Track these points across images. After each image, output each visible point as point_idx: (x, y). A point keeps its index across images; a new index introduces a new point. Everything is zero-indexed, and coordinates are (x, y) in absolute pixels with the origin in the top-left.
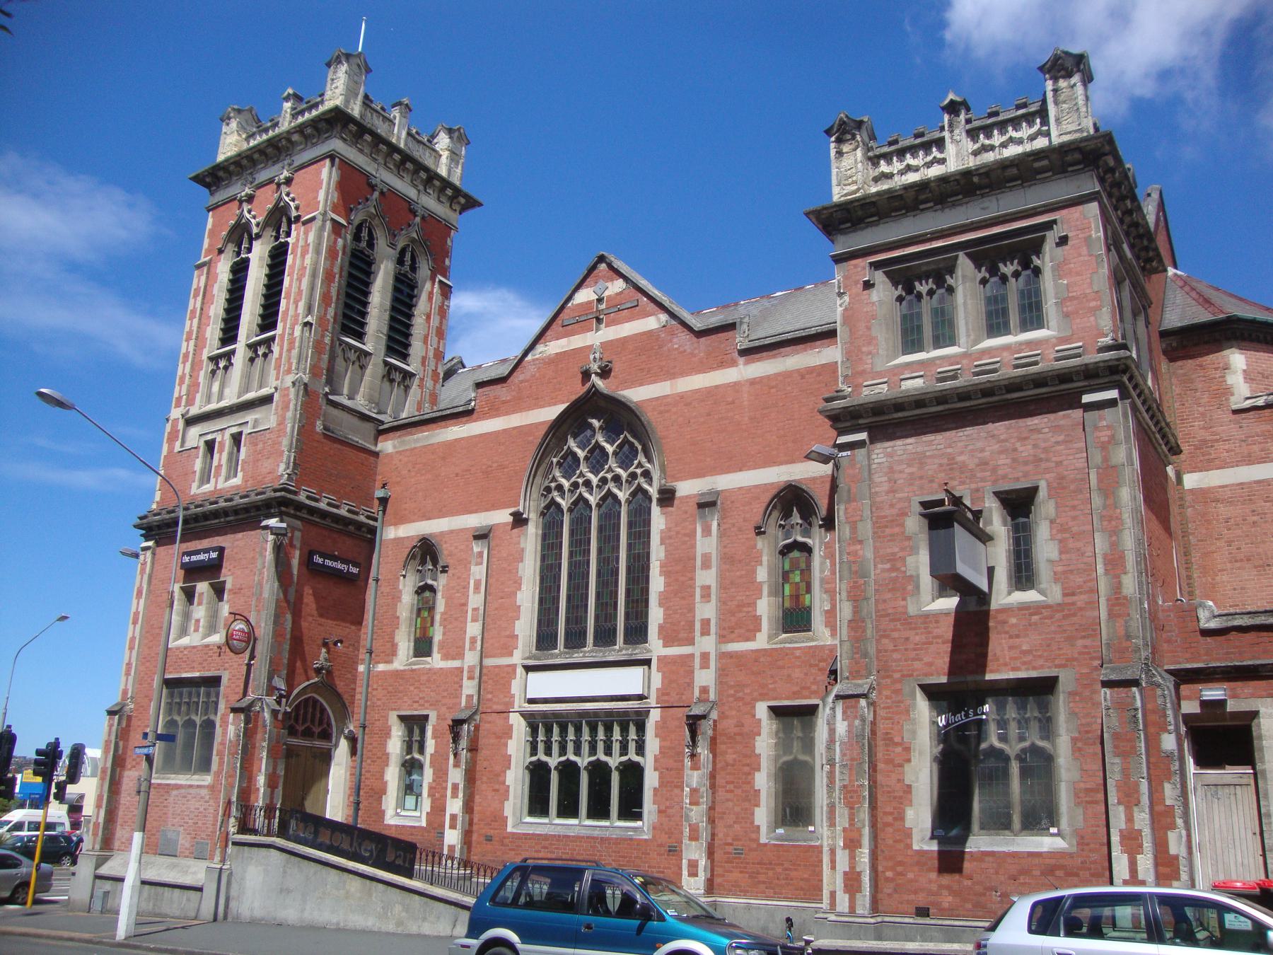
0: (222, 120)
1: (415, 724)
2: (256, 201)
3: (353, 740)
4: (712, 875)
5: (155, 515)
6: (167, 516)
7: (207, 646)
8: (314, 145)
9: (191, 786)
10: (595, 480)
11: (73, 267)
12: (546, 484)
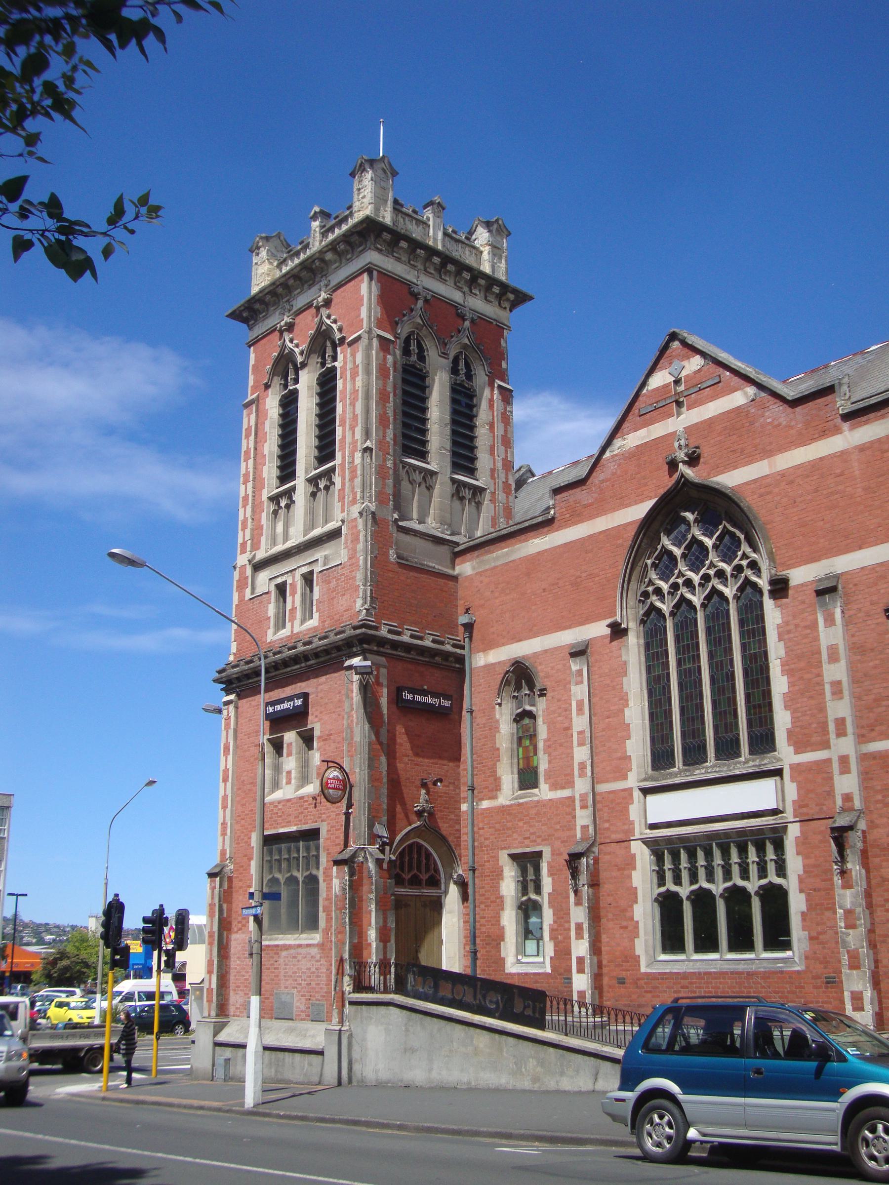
0: (251, 251)
1: (528, 862)
2: (296, 329)
3: (463, 885)
4: (881, 1008)
5: (234, 667)
6: (246, 667)
7: (302, 798)
8: (349, 260)
9: (300, 946)
10: (696, 578)
11: (109, 430)
12: (643, 588)
